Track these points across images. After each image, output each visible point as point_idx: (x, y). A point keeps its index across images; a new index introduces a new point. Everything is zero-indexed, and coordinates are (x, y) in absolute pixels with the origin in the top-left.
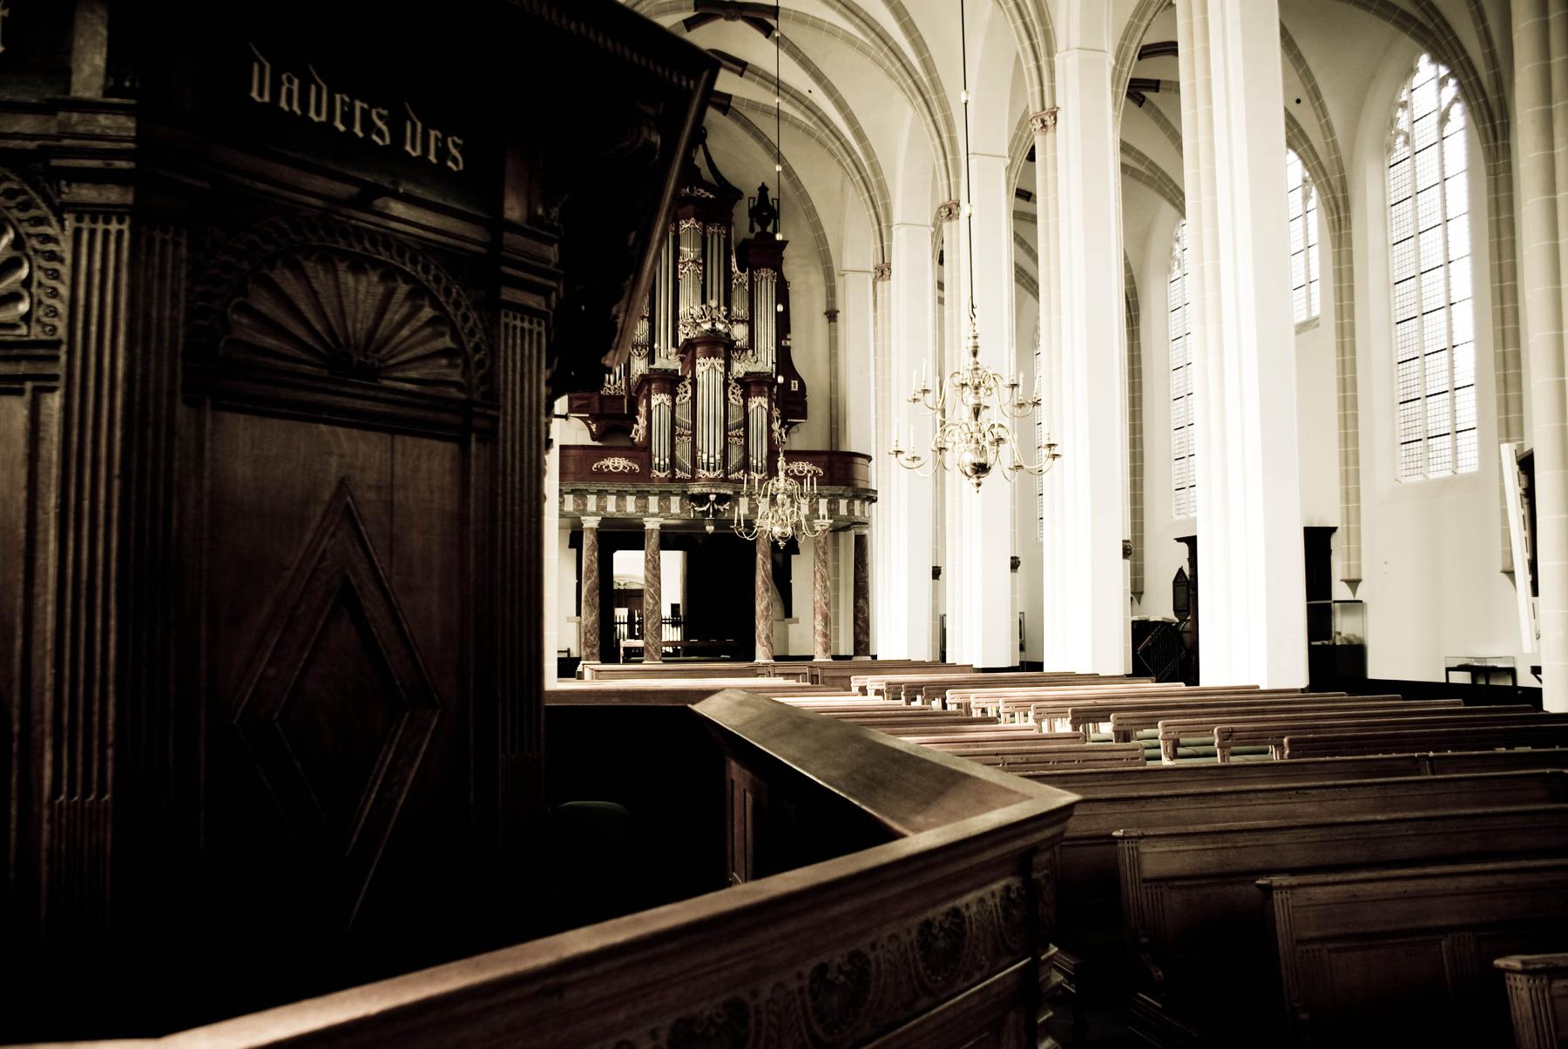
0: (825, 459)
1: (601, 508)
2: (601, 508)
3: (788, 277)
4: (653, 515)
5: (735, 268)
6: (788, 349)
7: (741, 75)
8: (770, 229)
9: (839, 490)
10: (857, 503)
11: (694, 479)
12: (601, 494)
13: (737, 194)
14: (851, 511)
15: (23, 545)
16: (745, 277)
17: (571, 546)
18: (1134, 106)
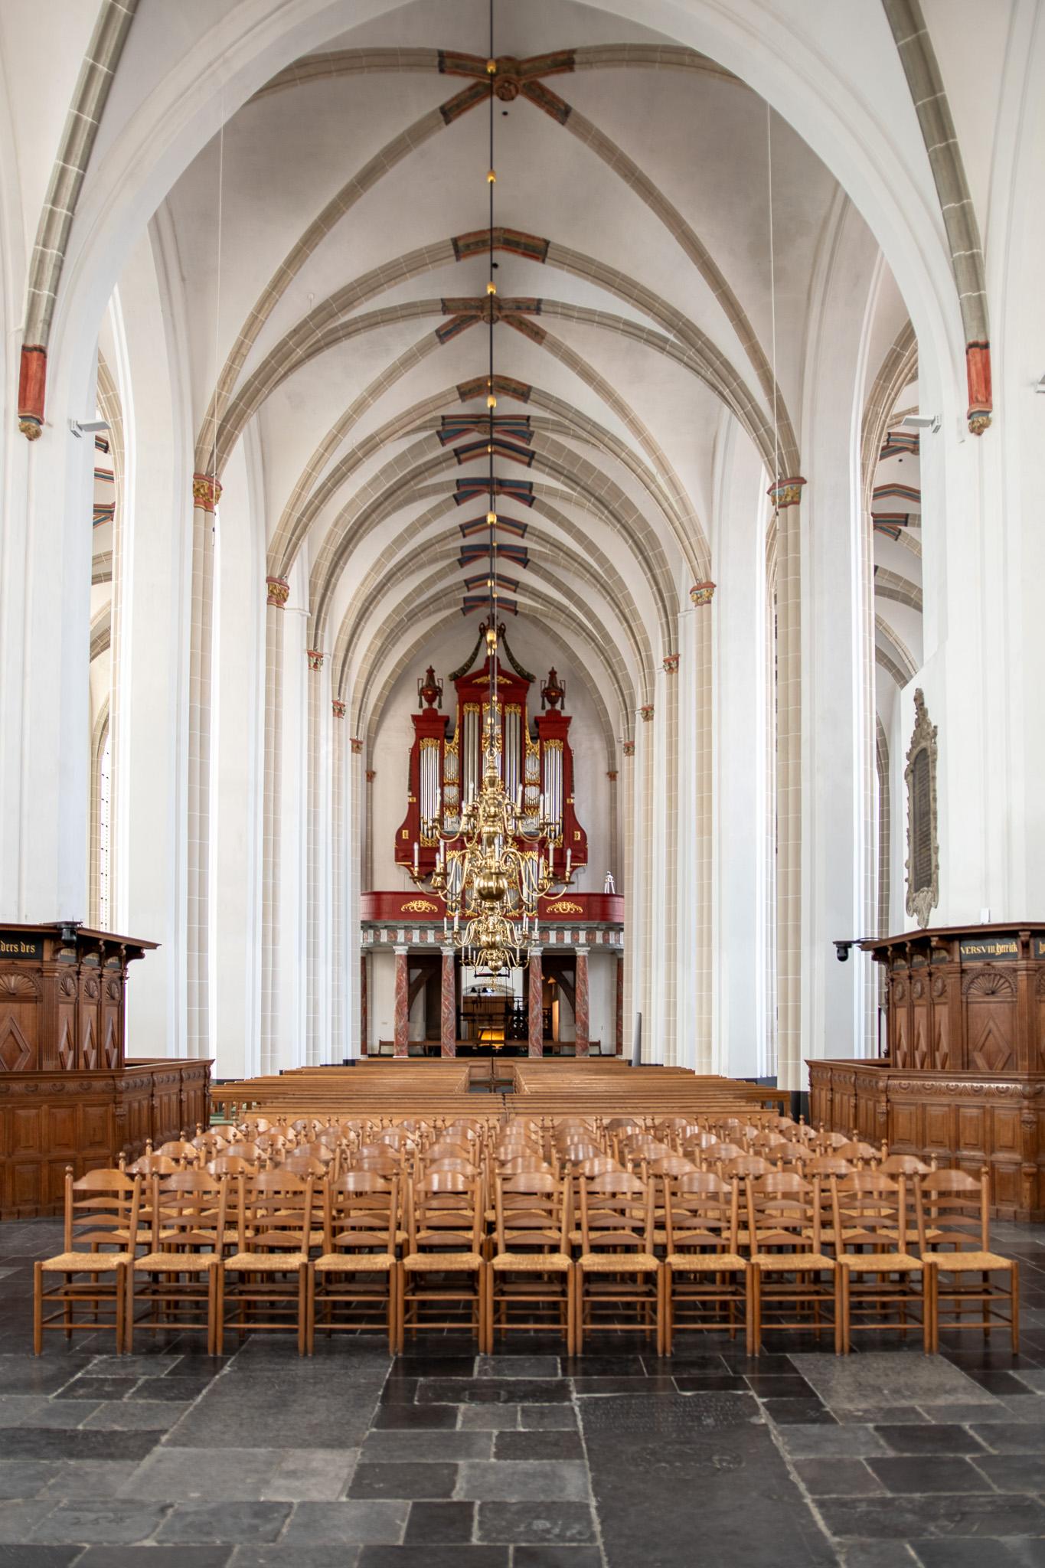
0: (584, 899)
1: (408, 939)
2: (408, 939)
3: (571, 745)
5: (528, 741)
6: (572, 805)
7: (529, 465)
8: (558, 707)
10: (612, 935)
13: (529, 679)
14: (606, 940)
15: (10, 961)
16: (537, 748)
17: (141, 956)
18: (888, 539)
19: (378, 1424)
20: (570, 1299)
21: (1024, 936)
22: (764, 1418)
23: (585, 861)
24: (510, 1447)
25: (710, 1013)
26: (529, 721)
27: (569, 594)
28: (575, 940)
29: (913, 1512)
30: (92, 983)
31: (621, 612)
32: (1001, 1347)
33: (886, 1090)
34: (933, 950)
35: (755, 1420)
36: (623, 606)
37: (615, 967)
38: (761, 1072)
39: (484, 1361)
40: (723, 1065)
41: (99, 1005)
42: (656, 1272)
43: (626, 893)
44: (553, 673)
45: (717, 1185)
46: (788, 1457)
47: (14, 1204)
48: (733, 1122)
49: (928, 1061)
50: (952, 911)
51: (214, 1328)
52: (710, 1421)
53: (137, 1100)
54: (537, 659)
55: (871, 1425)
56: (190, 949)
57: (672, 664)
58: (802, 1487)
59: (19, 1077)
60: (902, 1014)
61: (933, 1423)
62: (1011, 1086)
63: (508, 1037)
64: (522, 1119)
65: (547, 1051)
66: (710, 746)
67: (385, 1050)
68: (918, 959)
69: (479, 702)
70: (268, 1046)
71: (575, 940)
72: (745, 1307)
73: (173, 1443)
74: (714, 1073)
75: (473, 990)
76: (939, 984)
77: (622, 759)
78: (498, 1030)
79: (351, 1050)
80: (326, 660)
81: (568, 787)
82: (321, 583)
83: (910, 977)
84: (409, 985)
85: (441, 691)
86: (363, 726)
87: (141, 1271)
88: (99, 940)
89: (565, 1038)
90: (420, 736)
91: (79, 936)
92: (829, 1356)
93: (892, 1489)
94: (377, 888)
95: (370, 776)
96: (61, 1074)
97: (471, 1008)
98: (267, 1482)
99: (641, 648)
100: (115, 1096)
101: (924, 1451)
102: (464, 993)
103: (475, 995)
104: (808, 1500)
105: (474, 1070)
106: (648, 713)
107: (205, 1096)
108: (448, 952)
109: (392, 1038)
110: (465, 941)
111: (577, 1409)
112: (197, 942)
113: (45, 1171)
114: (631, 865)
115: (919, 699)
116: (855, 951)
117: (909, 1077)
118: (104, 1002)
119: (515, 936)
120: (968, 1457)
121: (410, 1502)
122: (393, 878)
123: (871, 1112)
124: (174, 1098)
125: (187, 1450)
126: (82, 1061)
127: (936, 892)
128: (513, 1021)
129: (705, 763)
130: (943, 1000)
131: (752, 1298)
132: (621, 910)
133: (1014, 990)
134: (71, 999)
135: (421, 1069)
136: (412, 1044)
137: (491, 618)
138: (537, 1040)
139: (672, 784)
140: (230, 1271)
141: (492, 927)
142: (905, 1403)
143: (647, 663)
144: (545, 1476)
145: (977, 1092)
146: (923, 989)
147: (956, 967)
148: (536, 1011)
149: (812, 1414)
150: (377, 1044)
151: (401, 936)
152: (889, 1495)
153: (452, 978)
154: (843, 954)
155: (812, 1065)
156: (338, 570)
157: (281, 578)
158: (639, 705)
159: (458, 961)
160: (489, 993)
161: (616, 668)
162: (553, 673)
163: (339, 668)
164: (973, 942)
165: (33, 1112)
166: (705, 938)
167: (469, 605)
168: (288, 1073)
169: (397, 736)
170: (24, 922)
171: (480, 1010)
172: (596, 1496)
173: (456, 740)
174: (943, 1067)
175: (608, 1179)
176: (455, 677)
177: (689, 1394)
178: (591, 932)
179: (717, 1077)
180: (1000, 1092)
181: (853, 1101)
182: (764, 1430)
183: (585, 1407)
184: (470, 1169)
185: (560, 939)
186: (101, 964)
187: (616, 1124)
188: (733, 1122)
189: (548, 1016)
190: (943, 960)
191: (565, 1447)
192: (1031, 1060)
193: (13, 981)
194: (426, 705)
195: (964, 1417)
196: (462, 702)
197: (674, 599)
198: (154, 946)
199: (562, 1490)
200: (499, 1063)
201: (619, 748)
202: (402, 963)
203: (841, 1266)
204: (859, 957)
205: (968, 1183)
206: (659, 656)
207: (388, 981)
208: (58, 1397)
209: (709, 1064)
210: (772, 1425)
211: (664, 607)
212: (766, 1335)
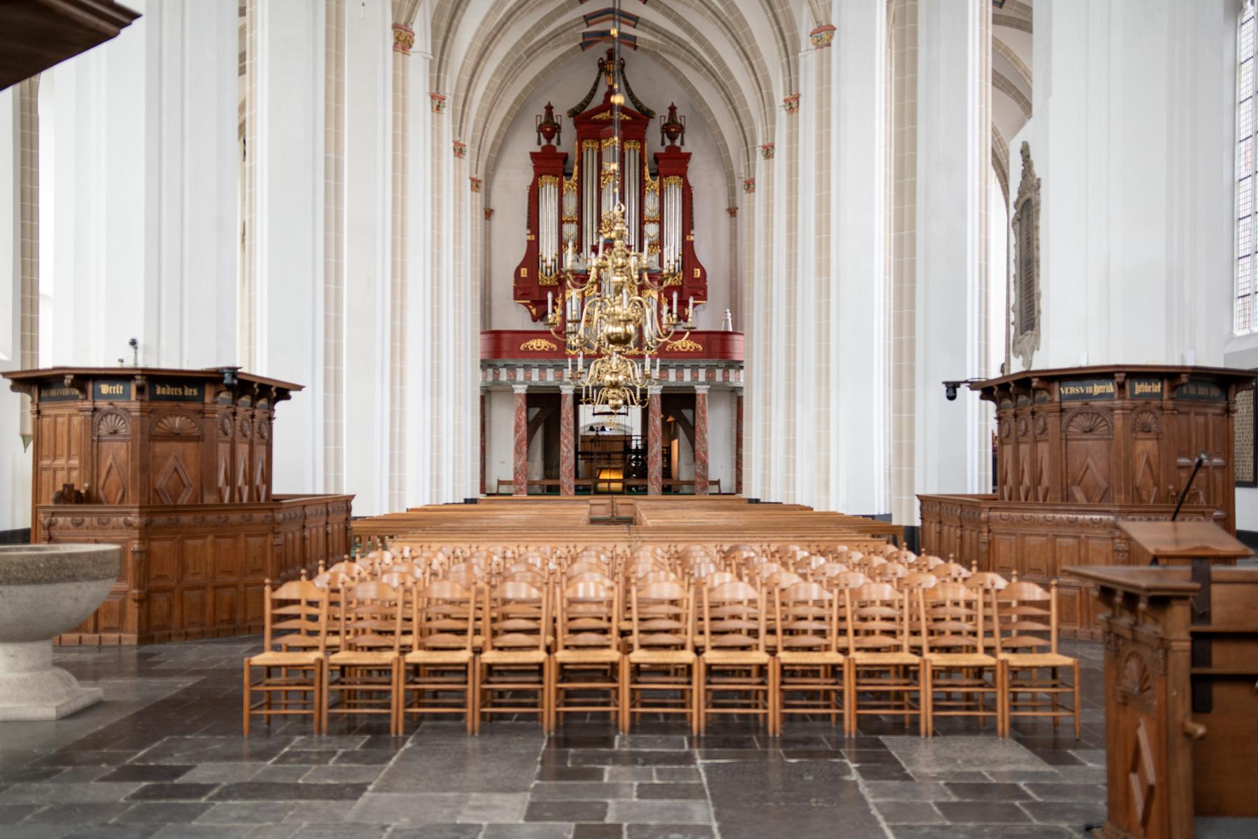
4: (568, 384)
5: (648, 178)
6: (692, 242)
8: (678, 143)
9: (713, 362)
10: (732, 372)
11: (70, 416)
12: (527, 368)
13: (648, 114)
15: (174, 404)
16: (657, 184)
17: (288, 398)
19: (541, 777)
20: (695, 687)
21: (1120, 378)
22: (855, 776)
23: (704, 297)
24: (646, 792)
25: (828, 450)
26: (648, 158)
27: (690, 30)
28: (695, 378)
29: (966, 833)
30: (246, 424)
31: (742, 49)
32: (1065, 735)
33: (988, 521)
34: (1036, 390)
35: (847, 778)
36: (745, 44)
37: (735, 405)
38: (879, 509)
39: (623, 739)
40: (842, 502)
41: (251, 444)
42: (766, 665)
43: (745, 331)
44: (673, 109)
45: (820, 593)
46: (871, 800)
47: (182, 626)
48: (843, 548)
49: (1031, 494)
50: (1057, 351)
51: (397, 713)
52: (810, 778)
53: (291, 532)
54: (658, 95)
55: (942, 782)
56: (326, 390)
57: (792, 103)
58: (880, 818)
59: (186, 509)
60: (1008, 451)
61: (995, 781)
62: (1104, 517)
63: (627, 475)
64: (649, 547)
65: (666, 490)
66: (828, 188)
67: (503, 489)
68: (1022, 399)
69: (598, 139)
70: (396, 487)
71: (695, 378)
72: (395, 45)
73: (378, 790)
74: (832, 509)
75: (592, 429)
76: (1041, 422)
77: (742, 197)
78: (616, 469)
79: (472, 491)
80: (449, 101)
81: (688, 224)
82: (444, 25)
83: (1016, 416)
84: (528, 424)
85: (559, 127)
86: (482, 164)
87: (334, 665)
88: (253, 383)
89: (684, 477)
90: (538, 174)
91: (240, 380)
92: (915, 738)
93: (951, 820)
94: (495, 327)
95: (488, 213)
96: (219, 507)
97: (589, 447)
98: (460, 813)
99: (762, 85)
100: (273, 528)
101: (975, 795)
102: (581, 432)
103: (593, 433)
104: (884, 825)
105: (595, 508)
106: (768, 151)
107: (347, 529)
108: (567, 391)
109: (511, 478)
110: (586, 382)
111: (701, 770)
112: (333, 383)
113: (210, 597)
114: (751, 303)
115: (1025, 152)
116: (963, 391)
117: (1032, 510)
118: (256, 441)
119: (634, 374)
120: (1017, 803)
121: (573, 825)
122: (515, 317)
123: (975, 542)
124: (321, 529)
125: (391, 795)
126: (237, 496)
127: (1038, 336)
128: (631, 461)
129: (823, 205)
130: (1043, 437)
131: (849, 686)
132: (739, 348)
133: (1111, 427)
134: (229, 438)
135: (543, 506)
136: (531, 484)
137: (611, 54)
138: (656, 479)
139: (792, 224)
140: (407, 664)
141: (615, 368)
142: (973, 769)
143: (766, 100)
144: (678, 809)
145: (1073, 523)
146: (1027, 427)
147: (1056, 406)
148: (656, 449)
149: (895, 774)
150: (495, 483)
151: (520, 375)
152: (948, 823)
153: (571, 416)
154: (951, 394)
155: (923, 499)
156: (459, 12)
157: (406, 24)
158: (760, 142)
159: (577, 398)
160: (607, 432)
161: (737, 104)
162: (673, 109)
163: (460, 108)
164: (1072, 383)
165: (200, 542)
166: (823, 377)
167: (588, 42)
168: (412, 510)
169: (516, 173)
170: (186, 367)
171: (600, 450)
172: (717, 820)
173: (575, 177)
174: (1045, 500)
175: (726, 588)
176: (574, 113)
177: (794, 761)
178: (710, 370)
179: (835, 513)
180: (1094, 522)
181: (959, 532)
182: (855, 785)
183: (708, 769)
184: (608, 583)
185: (680, 377)
186: (253, 405)
187: (734, 549)
188: (843, 548)
189: (667, 455)
190: (1044, 400)
191: (691, 792)
192: (1127, 493)
193: (177, 422)
194: (544, 142)
195: (1021, 779)
196: (581, 139)
197: (795, 39)
198: (299, 388)
199: (691, 818)
200: (619, 501)
201: (740, 185)
202: (521, 402)
203: (925, 661)
204: (970, 398)
205: (1037, 593)
206: (780, 95)
207: (508, 421)
208: (275, 763)
209: (828, 501)
210: (860, 781)
211: (785, 46)
212: (861, 720)
